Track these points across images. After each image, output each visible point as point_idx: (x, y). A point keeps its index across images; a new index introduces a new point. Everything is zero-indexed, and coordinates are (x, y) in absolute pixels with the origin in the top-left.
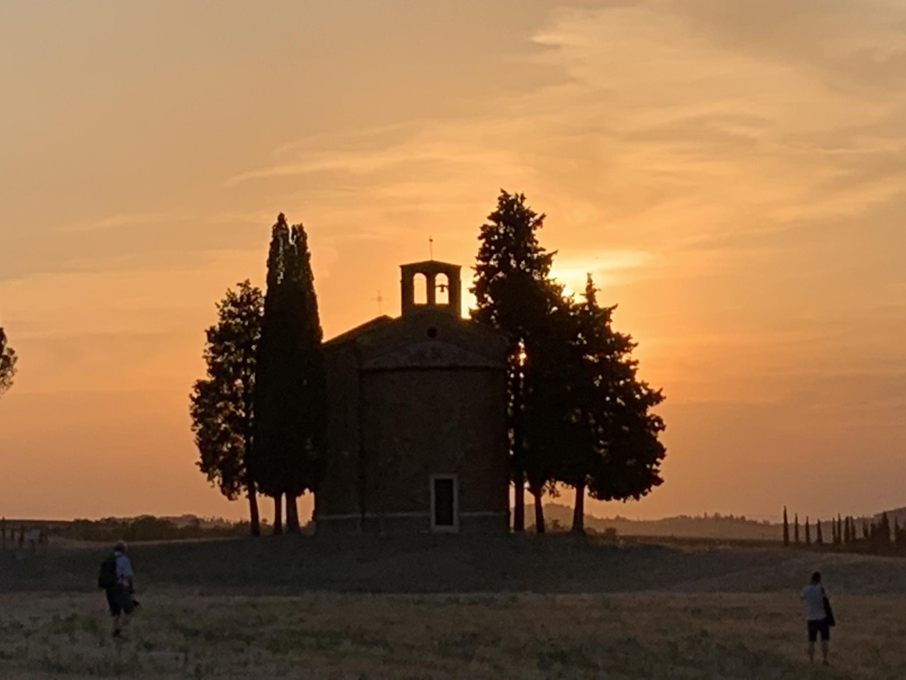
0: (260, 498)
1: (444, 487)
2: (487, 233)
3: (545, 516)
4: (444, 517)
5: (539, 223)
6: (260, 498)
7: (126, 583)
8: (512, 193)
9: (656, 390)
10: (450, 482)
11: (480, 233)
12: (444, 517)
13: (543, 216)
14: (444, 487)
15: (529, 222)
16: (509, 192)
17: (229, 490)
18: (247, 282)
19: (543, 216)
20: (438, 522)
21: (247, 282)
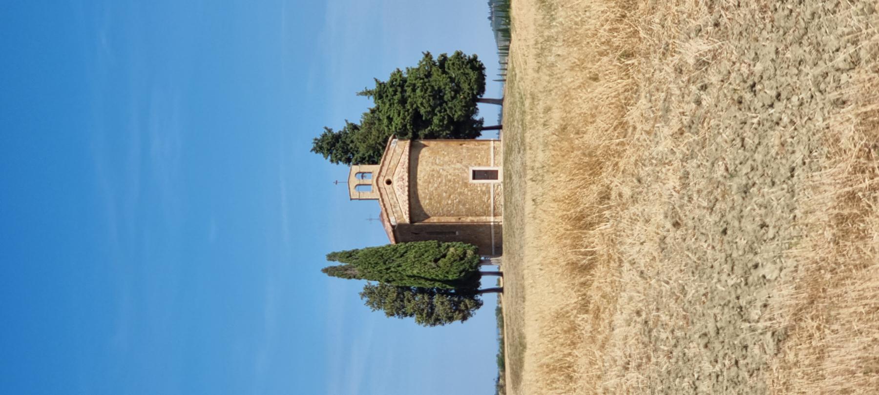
0: (483, 287)
1: (476, 175)
2: (338, 160)
3: (420, 192)
4: (493, 175)
5: (330, 131)
6: (483, 287)
7: (463, 274)
8: (312, 146)
9: (423, 56)
10: (474, 172)
11: (335, 164)
12: (493, 175)
13: (326, 128)
14: (476, 175)
15: (489, 263)
16: (312, 147)
17: (478, 304)
18: (360, 294)
19: (326, 128)
20: (496, 178)
21: (360, 294)
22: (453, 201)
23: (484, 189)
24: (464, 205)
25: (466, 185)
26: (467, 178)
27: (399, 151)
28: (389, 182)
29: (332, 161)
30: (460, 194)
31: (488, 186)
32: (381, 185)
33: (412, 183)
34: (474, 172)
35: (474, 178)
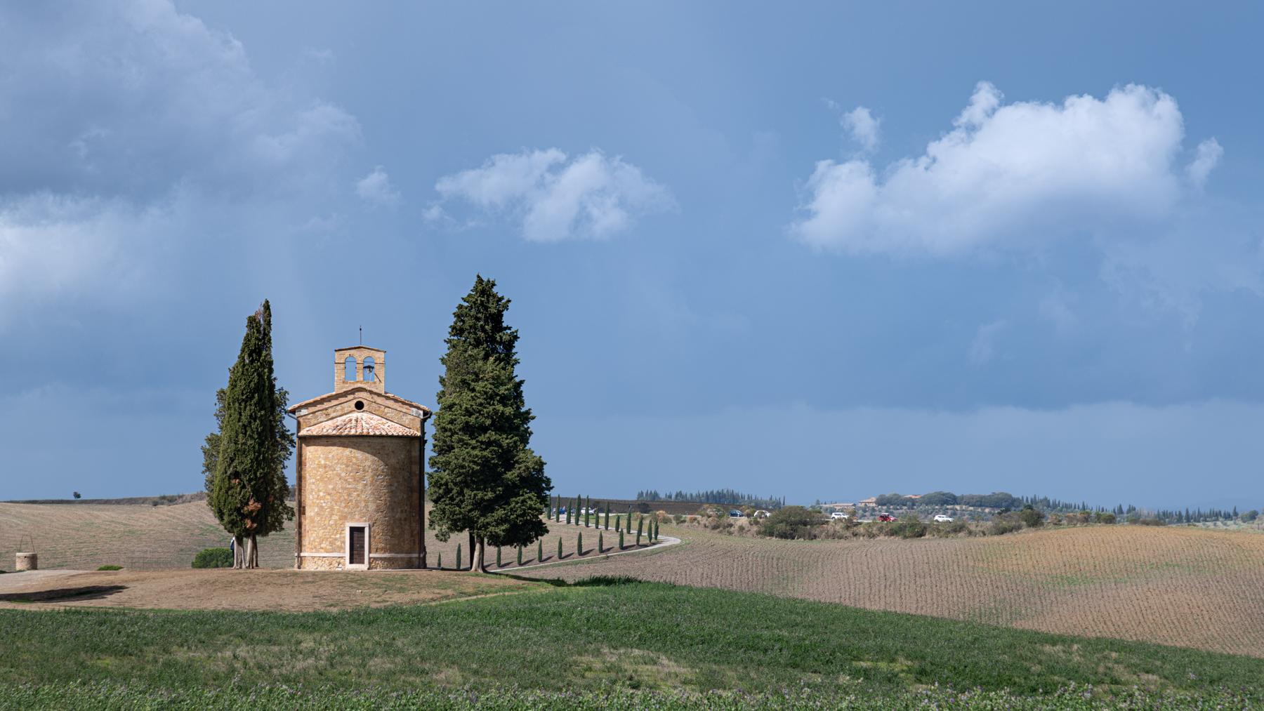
5: (506, 307)
20: (351, 562)
22: (323, 498)
23: (338, 543)
24: (318, 514)
25: (344, 518)
26: (352, 519)
27: (406, 420)
28: (359, 406)
29: (460, 307)
30: (332, 509)
31: (341, 548)
32: (357, 395)
33: (346, 441)
34: (361, 530)
35: (353, 530)
